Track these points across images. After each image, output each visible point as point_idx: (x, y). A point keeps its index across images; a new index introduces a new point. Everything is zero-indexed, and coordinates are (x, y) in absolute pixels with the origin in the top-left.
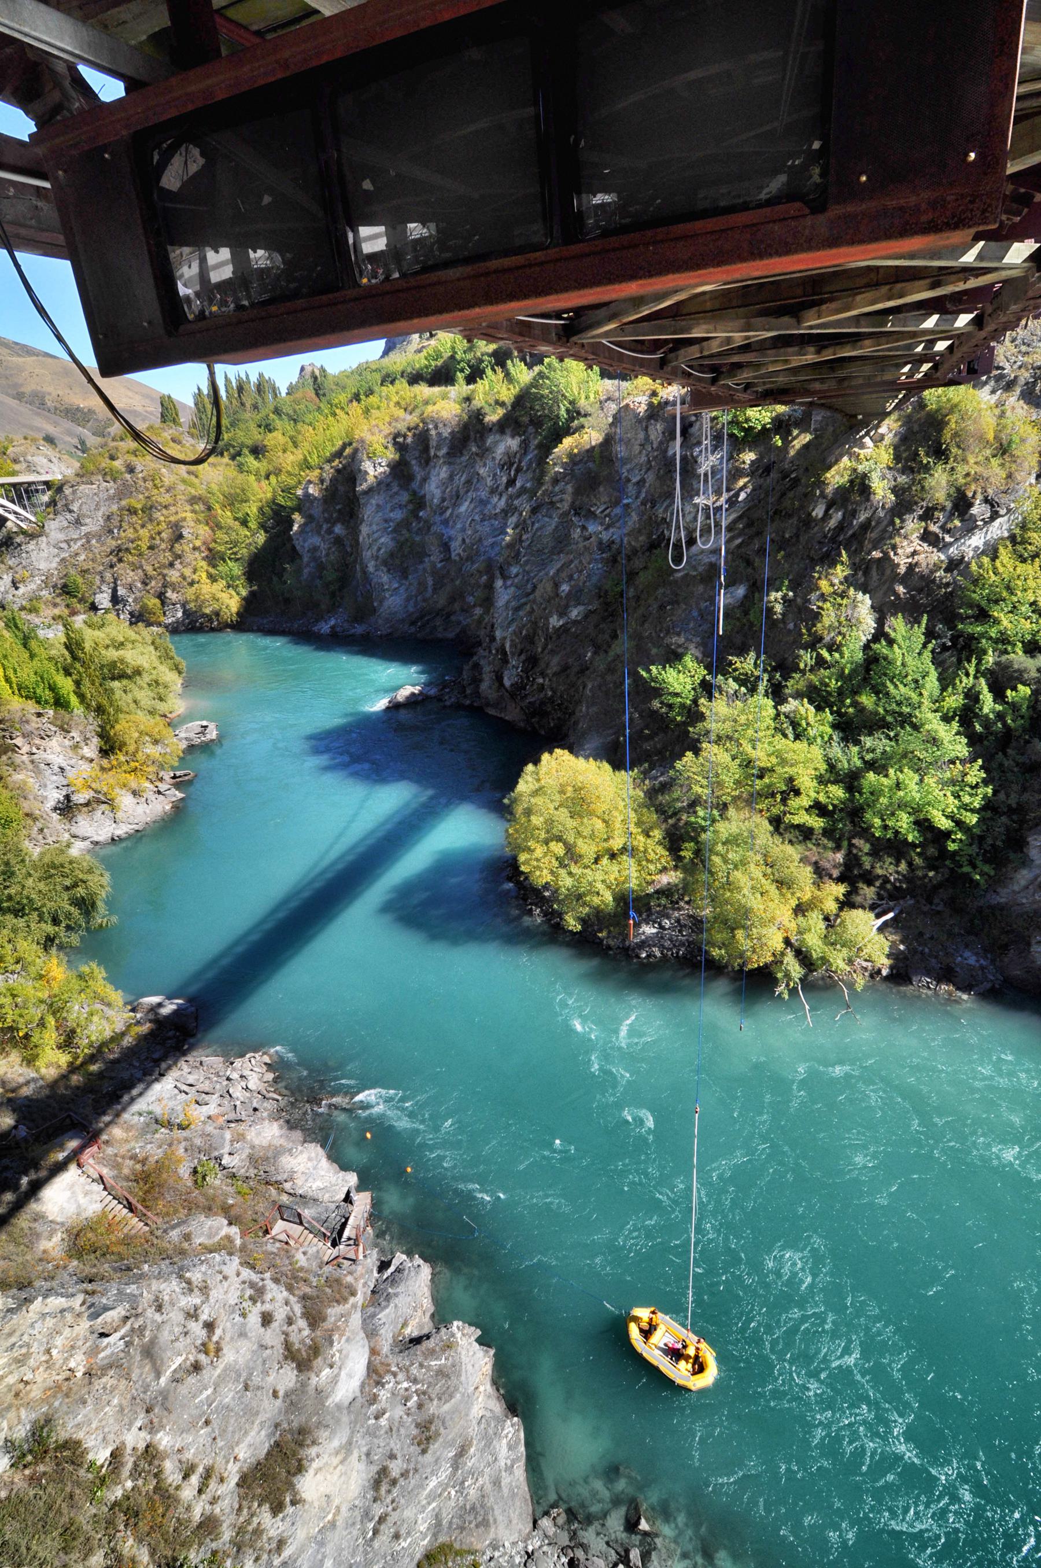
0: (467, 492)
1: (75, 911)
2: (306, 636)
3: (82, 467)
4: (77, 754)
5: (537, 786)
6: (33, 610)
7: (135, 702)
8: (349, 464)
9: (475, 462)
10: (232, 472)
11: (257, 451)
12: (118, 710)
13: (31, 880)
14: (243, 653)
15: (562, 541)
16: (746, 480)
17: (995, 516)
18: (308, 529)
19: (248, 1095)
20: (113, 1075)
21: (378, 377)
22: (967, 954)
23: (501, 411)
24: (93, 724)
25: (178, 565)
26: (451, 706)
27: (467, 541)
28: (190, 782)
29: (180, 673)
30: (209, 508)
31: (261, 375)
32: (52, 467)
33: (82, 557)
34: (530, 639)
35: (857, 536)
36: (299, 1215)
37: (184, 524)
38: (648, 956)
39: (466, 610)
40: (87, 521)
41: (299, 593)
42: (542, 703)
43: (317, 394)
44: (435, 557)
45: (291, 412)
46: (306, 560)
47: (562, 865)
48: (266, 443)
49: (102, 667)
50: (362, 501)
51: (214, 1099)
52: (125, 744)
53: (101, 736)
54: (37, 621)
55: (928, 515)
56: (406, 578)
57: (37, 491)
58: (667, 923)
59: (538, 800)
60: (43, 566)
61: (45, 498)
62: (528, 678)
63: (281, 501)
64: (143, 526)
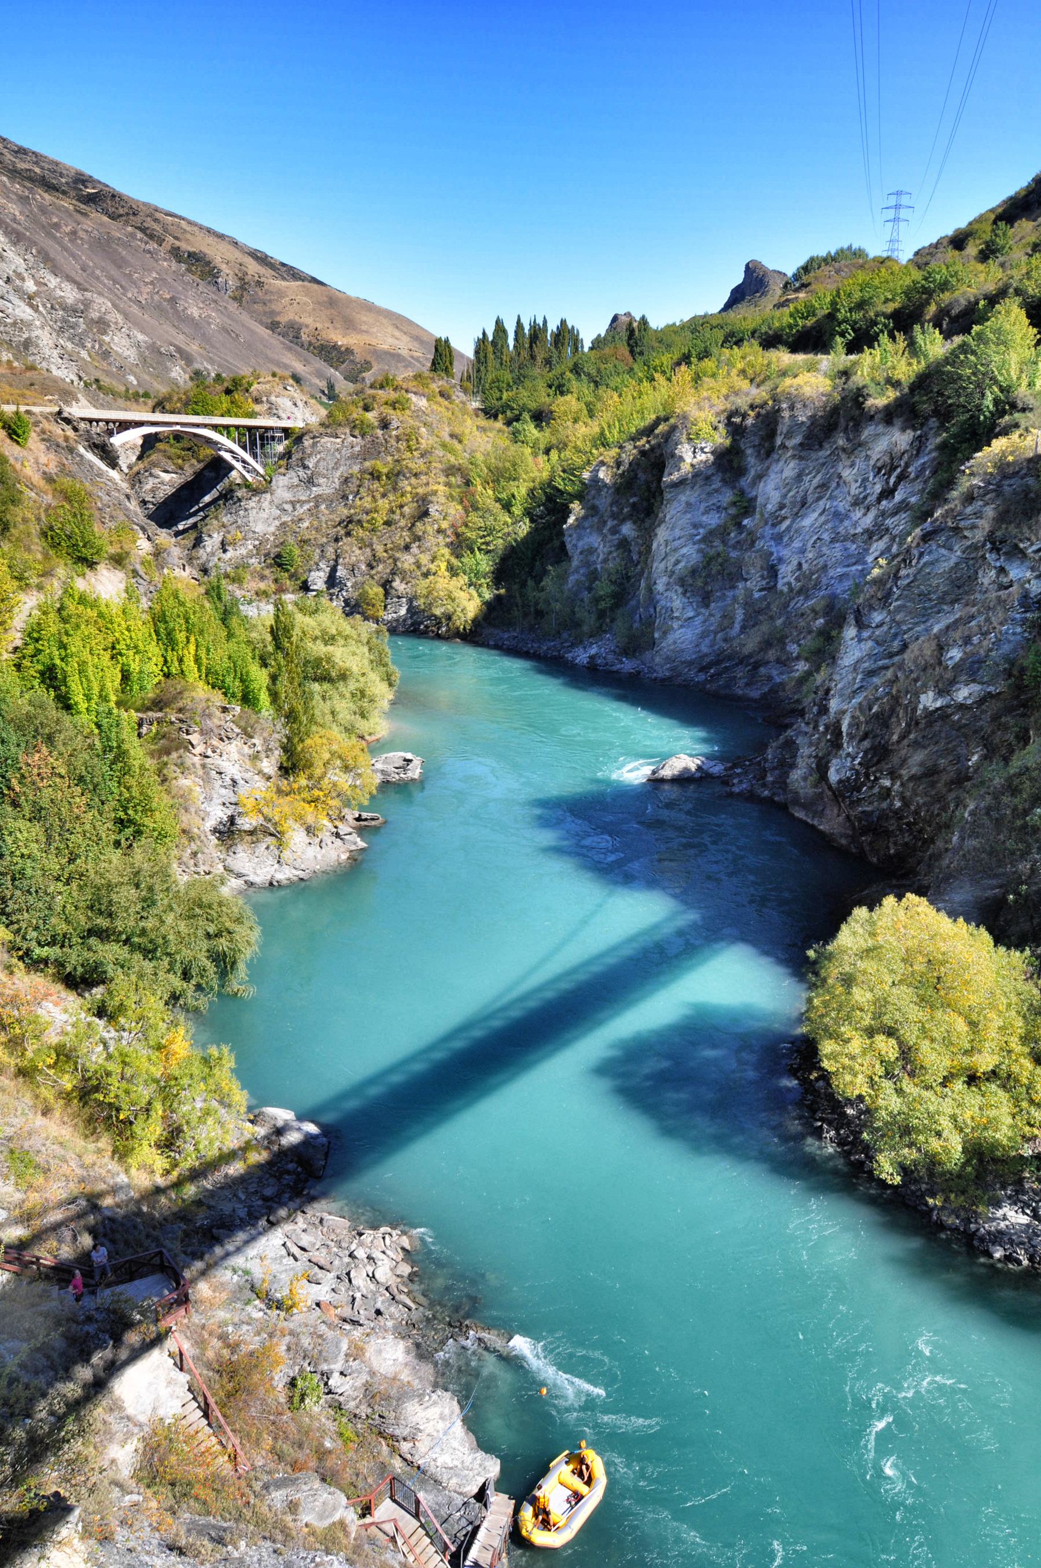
0: (819, 499)
1: (211, 968)
2: (554, 665)
3: (330, 415)
4: (254, 766)
5: (870, 943)
6: (237, 580)
7: (333, 713)
8: (659, 445)
9: (839, 459)
10: (504, 441)
11: (540, 417)
12: (312, 720)
13: (172, 915)
14: (472, 675)
15: (961, 585)
18: (586, 524)
19: (372, 1287)
20: (212, 1203)
21: (720, 335)
23: (892, 394)
24: (280, 732)
25: (414, 549)
26: (740, 794)
27: (805, 566)
28: (377, 829)
29: (390, 685)
30: (468, 483)
31: (563, 322)
32: (296, 411)
33: (306, 524)
34: (883, 720)
36: (418, 1502)
37: (434, 499)
38: (1008, 1258)
39: (785, 662)
40: (322, 481)
41: (558, 606)
42: (883, 816)
43: (632, 352)
44: (754, 583)
45: (594, 372)
46: (575, 563)
47: (888, 1075)
48: (553, 408)
49: (307, 662)
50: (667, 496)
51: (329, 1279)
52: (311, 765)
53: (285, 749)
54: (238, 593)
56: (707, 606)
57: (273, 438)
59: (867, 965)
60: (260, 528)
61: (280, 448)
62: (867, 776)
63: (559, 484)
64: (384, 495)
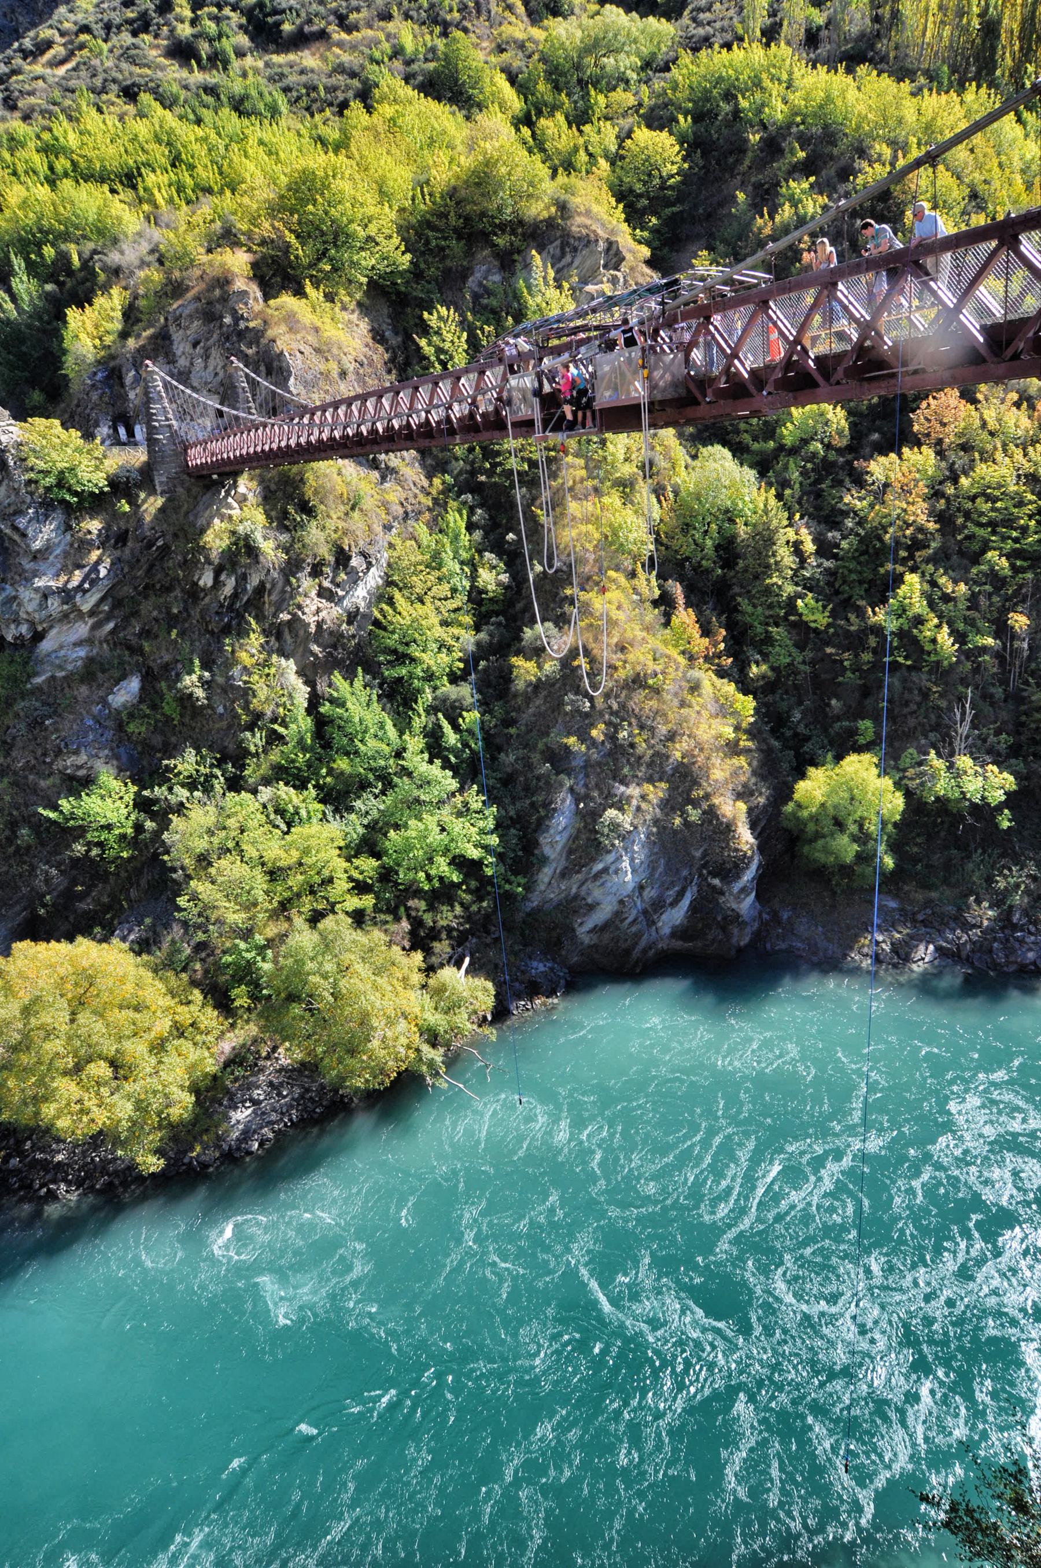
16: (98, 552)
17: (369, 565)
22: (535, 964)
35: (253, 602)
38: (261, 1145)
55: (316, 571)
58: (258, 1094)
